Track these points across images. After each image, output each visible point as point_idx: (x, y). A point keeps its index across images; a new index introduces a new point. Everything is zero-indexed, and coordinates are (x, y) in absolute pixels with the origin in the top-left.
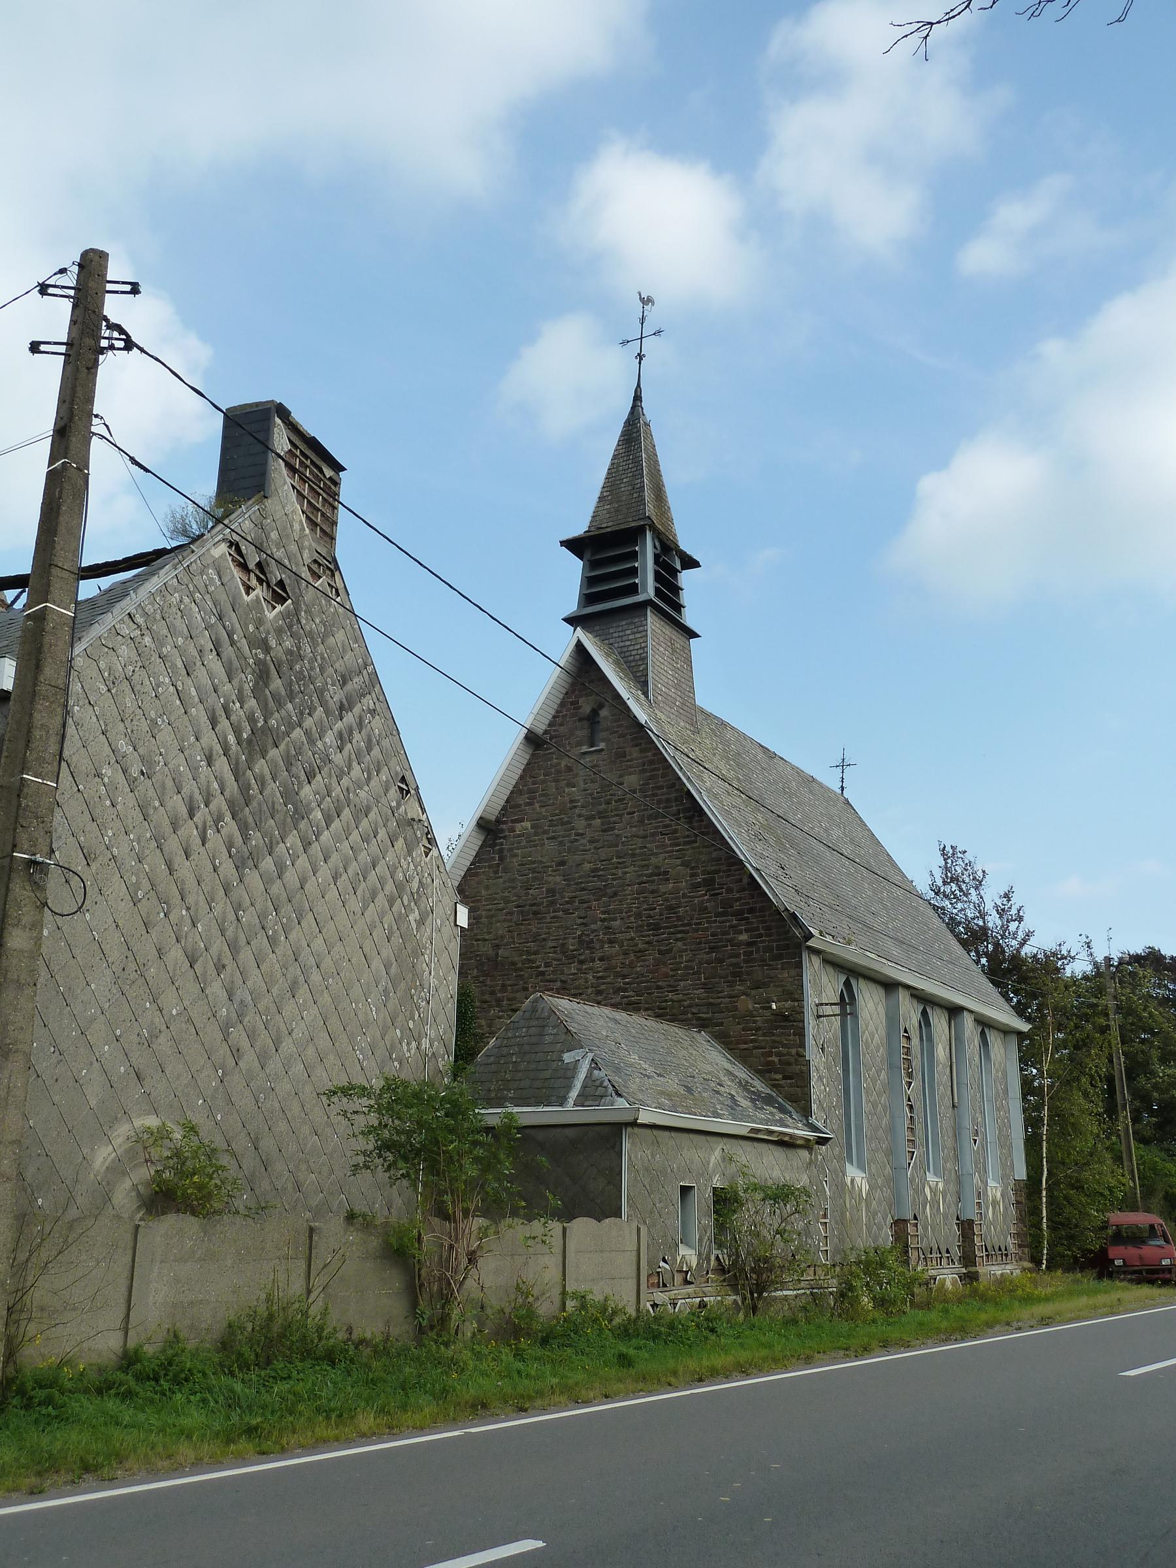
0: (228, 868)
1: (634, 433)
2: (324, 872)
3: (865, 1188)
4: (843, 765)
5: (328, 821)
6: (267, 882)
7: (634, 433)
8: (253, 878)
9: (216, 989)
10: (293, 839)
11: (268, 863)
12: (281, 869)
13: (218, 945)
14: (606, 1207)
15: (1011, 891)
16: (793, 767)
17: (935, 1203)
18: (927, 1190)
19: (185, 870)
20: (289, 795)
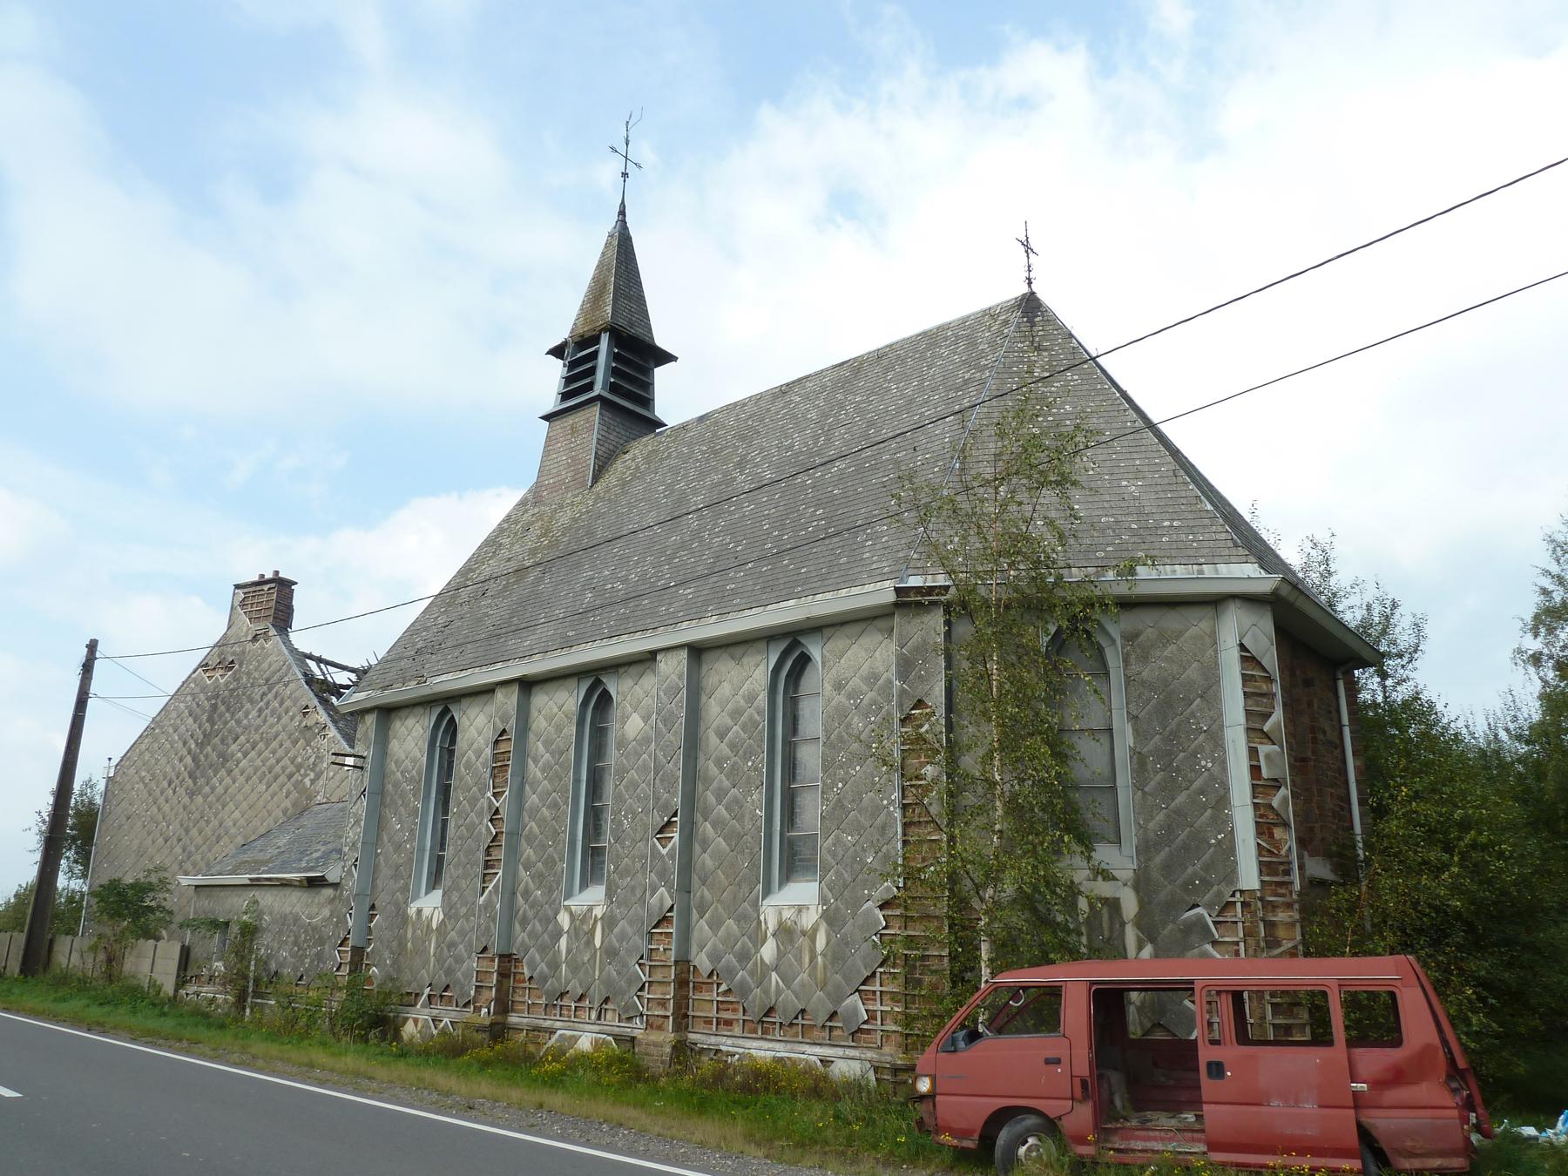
0: (186, 800)
2: (241, 779)
3: (438, 917)
5: (245, 755)
6: (206, 797)
8: (199, 799)
9: (178, 850)
10: (223, 772)
12: (213, 789)
19: (166, 808)
20: (222, 755)
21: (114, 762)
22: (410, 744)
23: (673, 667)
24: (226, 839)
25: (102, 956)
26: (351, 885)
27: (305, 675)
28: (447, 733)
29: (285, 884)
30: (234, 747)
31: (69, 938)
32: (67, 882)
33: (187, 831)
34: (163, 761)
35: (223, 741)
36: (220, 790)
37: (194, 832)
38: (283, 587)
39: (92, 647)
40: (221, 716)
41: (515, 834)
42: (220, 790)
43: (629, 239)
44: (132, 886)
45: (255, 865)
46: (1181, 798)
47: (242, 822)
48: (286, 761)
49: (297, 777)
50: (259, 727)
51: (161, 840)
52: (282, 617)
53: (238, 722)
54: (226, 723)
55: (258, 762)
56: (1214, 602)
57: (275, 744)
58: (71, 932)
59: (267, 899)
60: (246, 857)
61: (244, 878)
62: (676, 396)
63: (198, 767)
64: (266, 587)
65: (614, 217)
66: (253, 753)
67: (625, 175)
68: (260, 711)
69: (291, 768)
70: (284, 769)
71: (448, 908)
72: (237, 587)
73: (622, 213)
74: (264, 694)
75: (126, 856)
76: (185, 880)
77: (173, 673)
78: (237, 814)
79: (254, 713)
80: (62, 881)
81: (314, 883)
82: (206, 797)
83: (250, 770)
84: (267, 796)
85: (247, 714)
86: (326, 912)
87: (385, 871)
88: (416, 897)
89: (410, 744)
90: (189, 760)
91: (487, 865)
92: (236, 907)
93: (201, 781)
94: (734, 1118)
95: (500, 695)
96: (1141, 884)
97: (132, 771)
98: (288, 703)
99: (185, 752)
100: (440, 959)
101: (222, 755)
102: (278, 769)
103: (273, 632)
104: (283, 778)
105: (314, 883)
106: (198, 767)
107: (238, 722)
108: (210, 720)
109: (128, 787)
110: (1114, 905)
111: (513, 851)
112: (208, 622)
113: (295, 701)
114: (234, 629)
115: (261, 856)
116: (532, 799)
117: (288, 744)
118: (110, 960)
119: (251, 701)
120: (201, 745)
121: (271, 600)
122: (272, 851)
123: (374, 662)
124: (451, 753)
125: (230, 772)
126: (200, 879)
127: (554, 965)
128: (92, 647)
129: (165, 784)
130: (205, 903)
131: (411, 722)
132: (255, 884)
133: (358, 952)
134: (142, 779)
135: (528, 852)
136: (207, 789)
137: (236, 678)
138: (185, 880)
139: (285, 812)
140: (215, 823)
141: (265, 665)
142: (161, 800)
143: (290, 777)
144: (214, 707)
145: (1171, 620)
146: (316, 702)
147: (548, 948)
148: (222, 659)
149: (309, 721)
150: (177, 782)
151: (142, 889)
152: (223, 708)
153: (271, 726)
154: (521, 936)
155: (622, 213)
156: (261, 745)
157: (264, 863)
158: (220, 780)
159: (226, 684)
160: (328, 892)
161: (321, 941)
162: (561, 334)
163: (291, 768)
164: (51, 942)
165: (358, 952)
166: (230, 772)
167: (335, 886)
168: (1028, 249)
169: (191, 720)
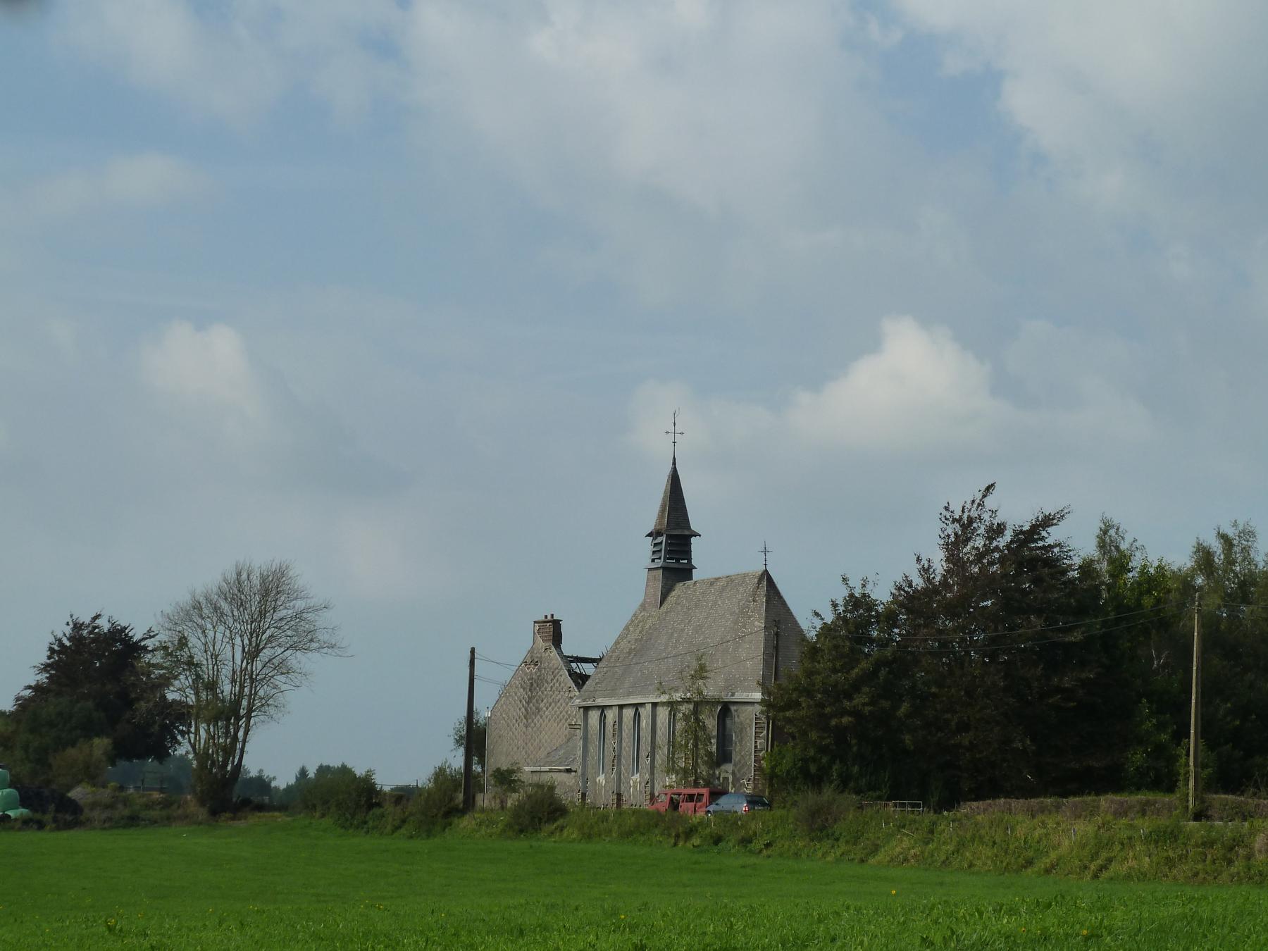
23: (649, 707)
29: (560, 771)
32: (477, 768)
38: (556, 624)
39: (473, 651)
45: (550, 763)
52: (557, 639)
56: (752, 703)
58: (482, 791)
59: (555, 775)
61: (547, 768)
62: (706, 558)
71: (606, 779)
73: (674, 463)
76: (527, 769)
81: (569, 771)
92: (546, 778)
94: (282, 668)
96: (733, 773)
105: (569, 771)
110: (727, 779)
111: (619, 761)
112: (523, 640)
120: (528, 703)
121: (553, 631)
123: (605, 652)
128: (473, 651)
130: (535, 778)
132: (551, 771)
138: (527, 769)
148: (533, 661)
149: (572, 694)
151: (510, 772)
155: (674, 463)
165: (584, 795)
168: (765, 552)
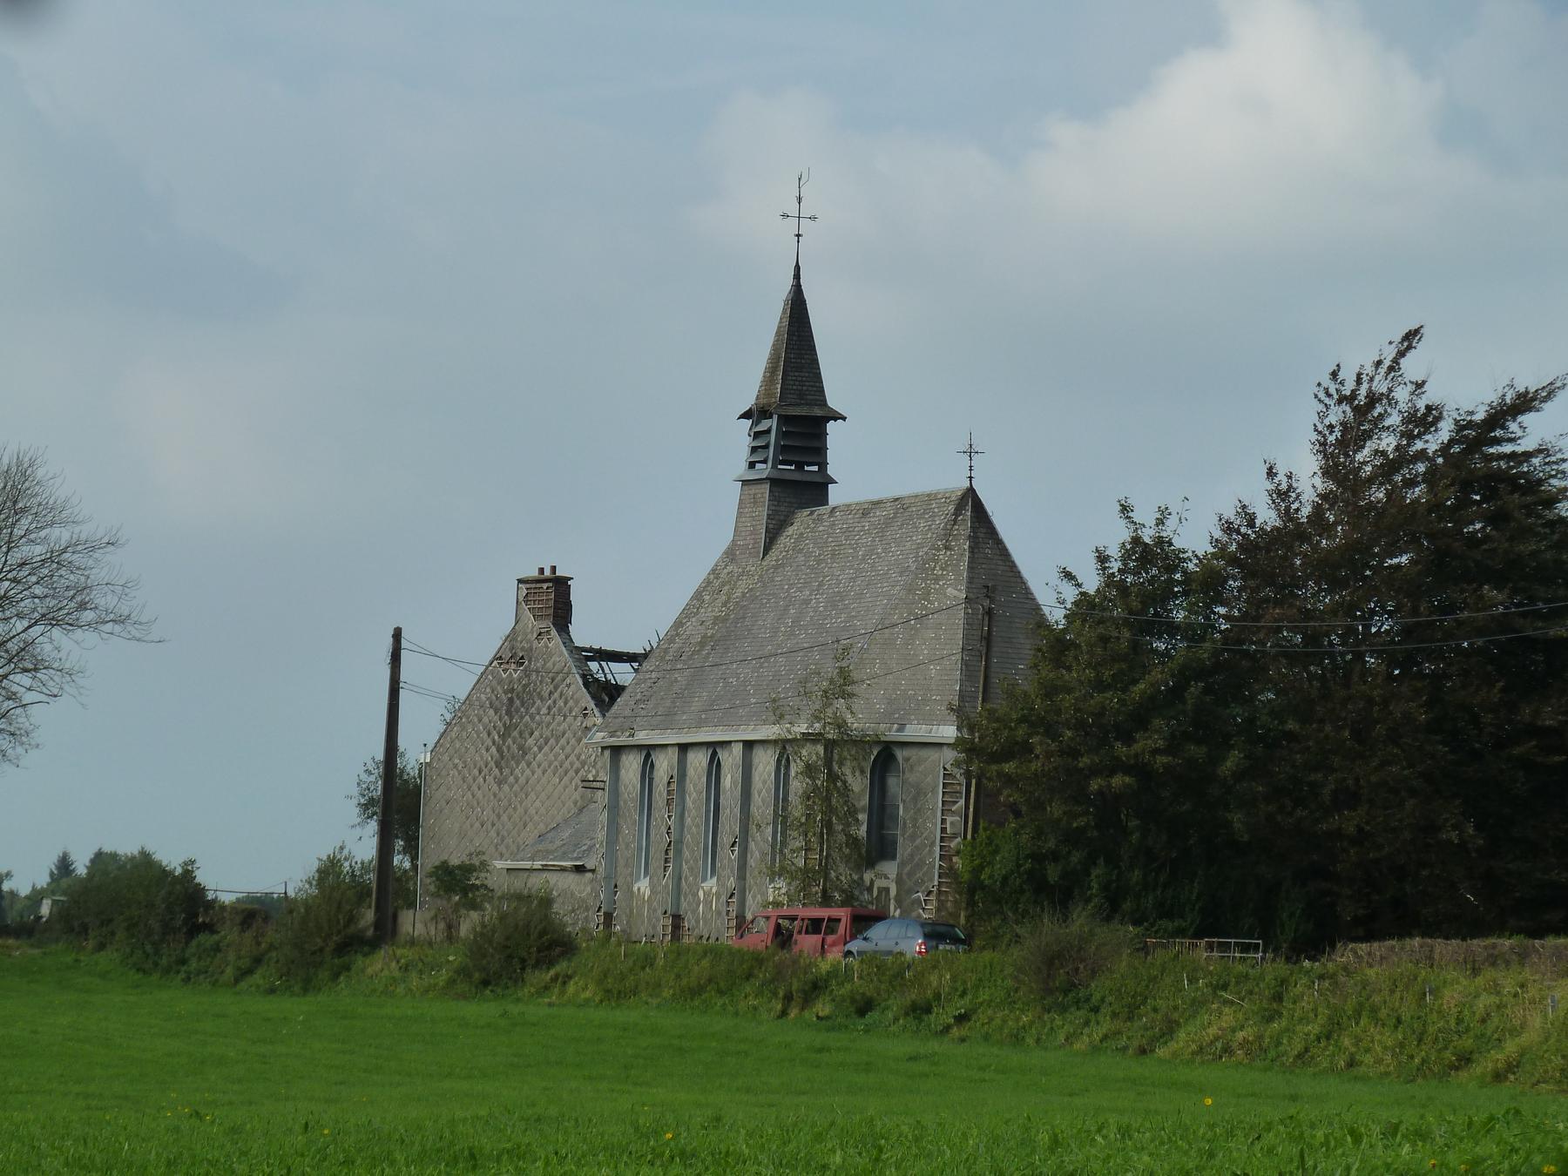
0: (495, 787)
1: (797, 310)
2: (539, 772)
3: (648, 893)
4: (971, 452)
5: (540, 749)
6: (511, 787)
7: (797, 310)
8: (506, 788)
9: (493, 833)
10: (523, 764)
11: (511, 779)
12: (517, 780)
13: (493, 817)
14: (894, 858)
15: (1424, 382)
16: (740, 514)
17: (708, 903)
18: (701, 894)
19: (479, 794)
20: (521, 748)
21: (430, 747)
22: (631, 774)
23: (737, 750)
24: (530, 826)
25: (442, 925)
26: (601, 871)
27: (584, 677)
28: (648, 768)
29: (563, 869)
30: (531, 741)
31: (411, 912)
33: (499, 816)
34: (472, 749)
35: (521, 733)
36: (522, 780)
37: (504, 818)
38: (561, 586)
39: (397, 635)
40: (517, 711)
41: (680, 842)
42: (522, 780)
43: (803, 302)
44: (459, 867)
45: (546, 854)
46: (918, 841)
47: (543, 810)
48: (572, 758)
49: (582, 772)
50: (549, 724)
51: (477, 825)
52: (561, 614)
53: (532, 718)
54: (522, 718)
55: (551, 757)
57: (563, 741)
58: (411, 905)
59: (553, 878)
60: (540, 847)
61: (538, 864)
63: (502, 757)
64: (545, 586)
65: (790, 281)
66: (546, 748)
67: (800, 200)
68: (549, 708)
69: (577, 764)
70: (572, 764)
72: (520, 581)
73: (797, 276)
74: (551, 693)
75: (447, 835)
76: (499, 864)
77: (462, 685)
78: (538, 803)
79: (544, 711)
80: (396, 860)
81: (580, 869)
82: (511, 787)
83: (545, 764)
84: (560, 788)
85: (539, 710)
86: (589, 889)
87: (621, 862)
88: (638, 879)
89: (631, 774)
90: (494, 749)
91: (666, 861)
93: (506, 771)
95: (670, 750)
97: (446, 758)
98: (571, 703)
99: (489, 742)
100: (649, 920)
101: (521, 748)
102: (567, 764)
103: (554, 632)
104: (571, 773)
105: (580, 869)
106: (502, 757)
107: (532, 718)
108: (508, 713)
109: (444, 773)
110: (887, 890)
111: (679, 852)
112: (490, 618)
113: (577, 702)
114: (520, 625)
115: (551, 847)
116: (688, 821)
117: (573, 741)
118: (449, 927)
119: (542, 699)
120: (503, 737)
121: (552, 597)
122: (559, 843)
124: (651, 780)
125: (529, 764)
126: (510, 864)
127: (697, 922)
128: (397, 635)
129: (476, 772)
130: (518, 884)
131: (631, 757)
132: (545, 869)
133: (609, 917)
134: (456, 766)
135: (686, 853)
136: (511, 779)
137: (527, 673)
138: (499, 864)
139: (575, 803)
140: (520, 810)
141: (549, 665)
142: (475, 787)
143: (577, 772)
144: (511, 700)
145: (924, 753)
146: (592, 705)
147: (695, 911)
148: (513, 655)
150: (485, 771)
151: (467, 869)
152: (518, 702)
153: (559, 724)
154: (684, 905)
155: (797, 276)
156: (552, 741)
157: (552, 852)
158: (522, 771)
159: (519, 680)
160: (589, 875)
161: (587, 909)
162: (748, 402)
163: (577, 764)
164: (395, 917)
165: (609, 917)
166: (529, 764)
167: (593, 871)
169: (492, 712)
